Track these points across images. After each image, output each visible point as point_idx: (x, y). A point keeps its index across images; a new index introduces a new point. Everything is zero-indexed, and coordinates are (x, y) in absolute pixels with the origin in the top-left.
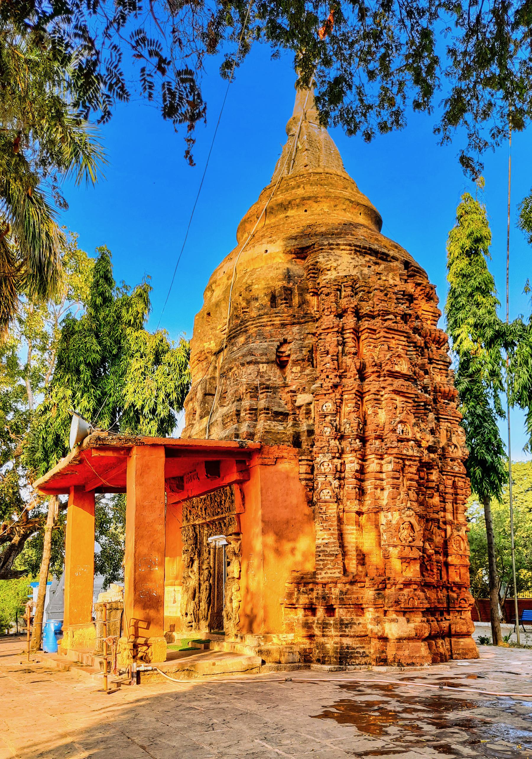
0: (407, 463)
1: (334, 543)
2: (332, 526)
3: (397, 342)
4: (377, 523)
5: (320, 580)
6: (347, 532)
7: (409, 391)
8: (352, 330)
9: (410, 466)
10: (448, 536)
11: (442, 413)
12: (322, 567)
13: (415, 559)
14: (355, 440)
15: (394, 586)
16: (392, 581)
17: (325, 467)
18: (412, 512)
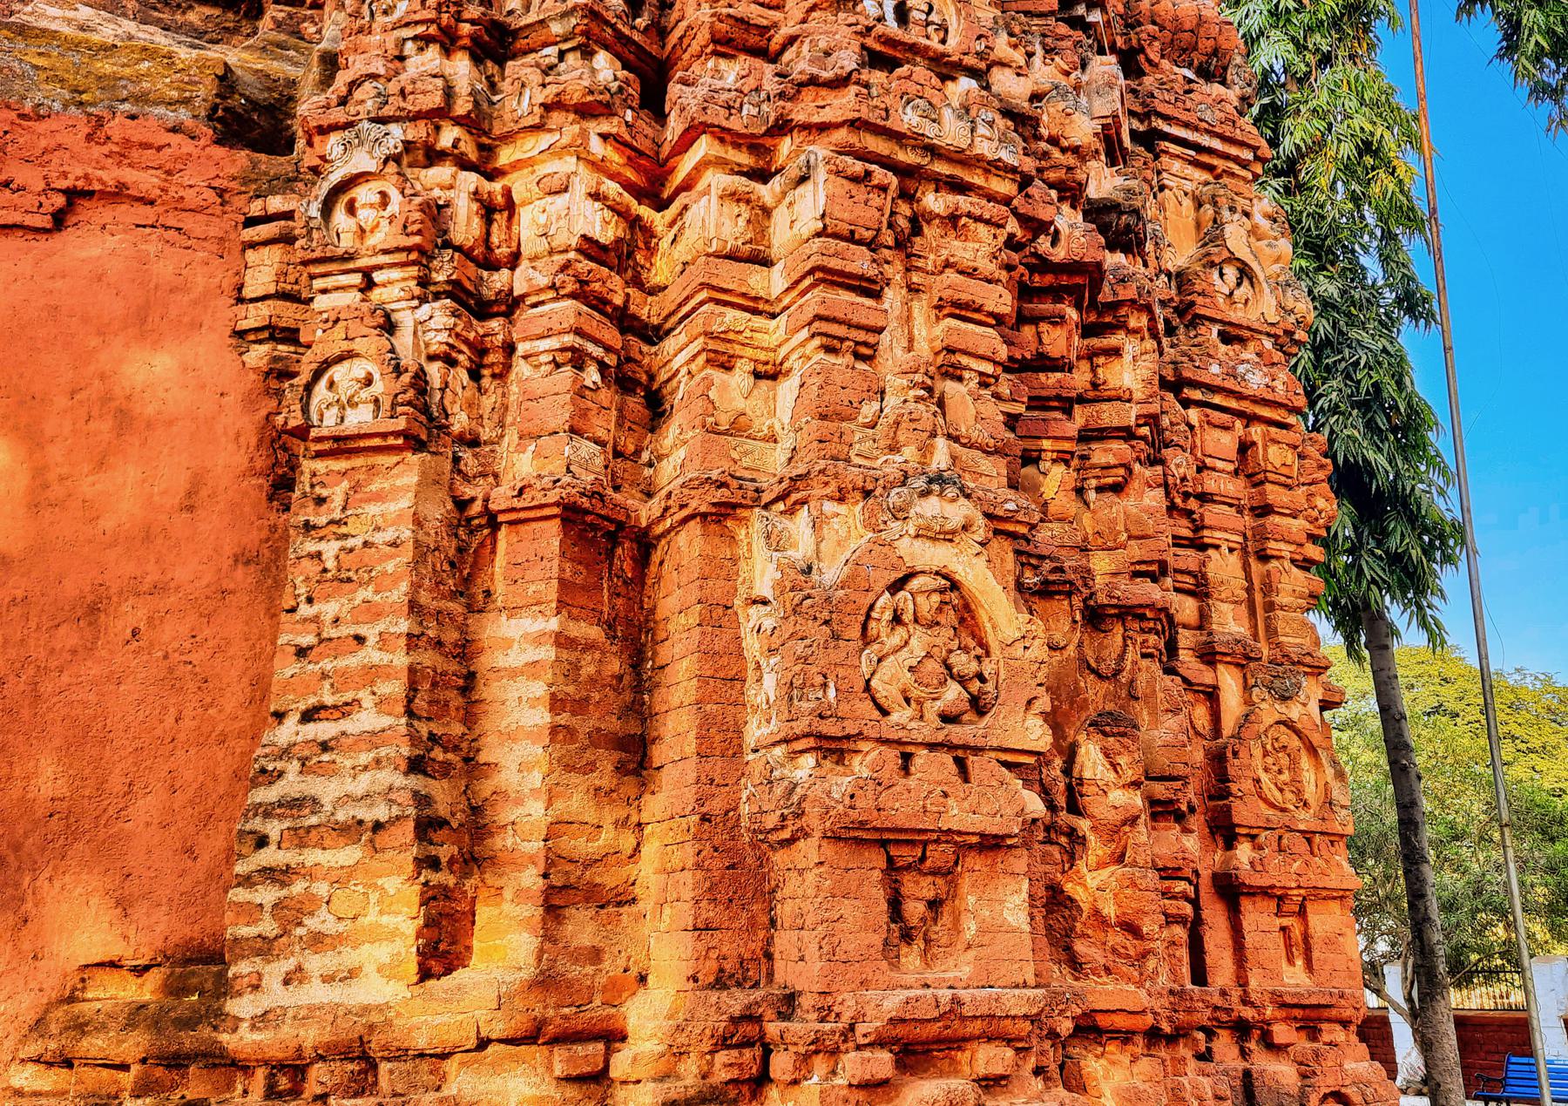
0: (934, 202)
1: (373, 738)
2: (372, 612)
4: (717, 589)
5: (242, 1040)
6: (501, 661)
9: (952, 220)
10: (1228, 724)
11: (1162, 108)
12: (268, 927)
13: (991, 844)
14: (588, 54)
15: (820, 1065)
16: (803, 1027)
17: (366, 215)
18: (957, 512)
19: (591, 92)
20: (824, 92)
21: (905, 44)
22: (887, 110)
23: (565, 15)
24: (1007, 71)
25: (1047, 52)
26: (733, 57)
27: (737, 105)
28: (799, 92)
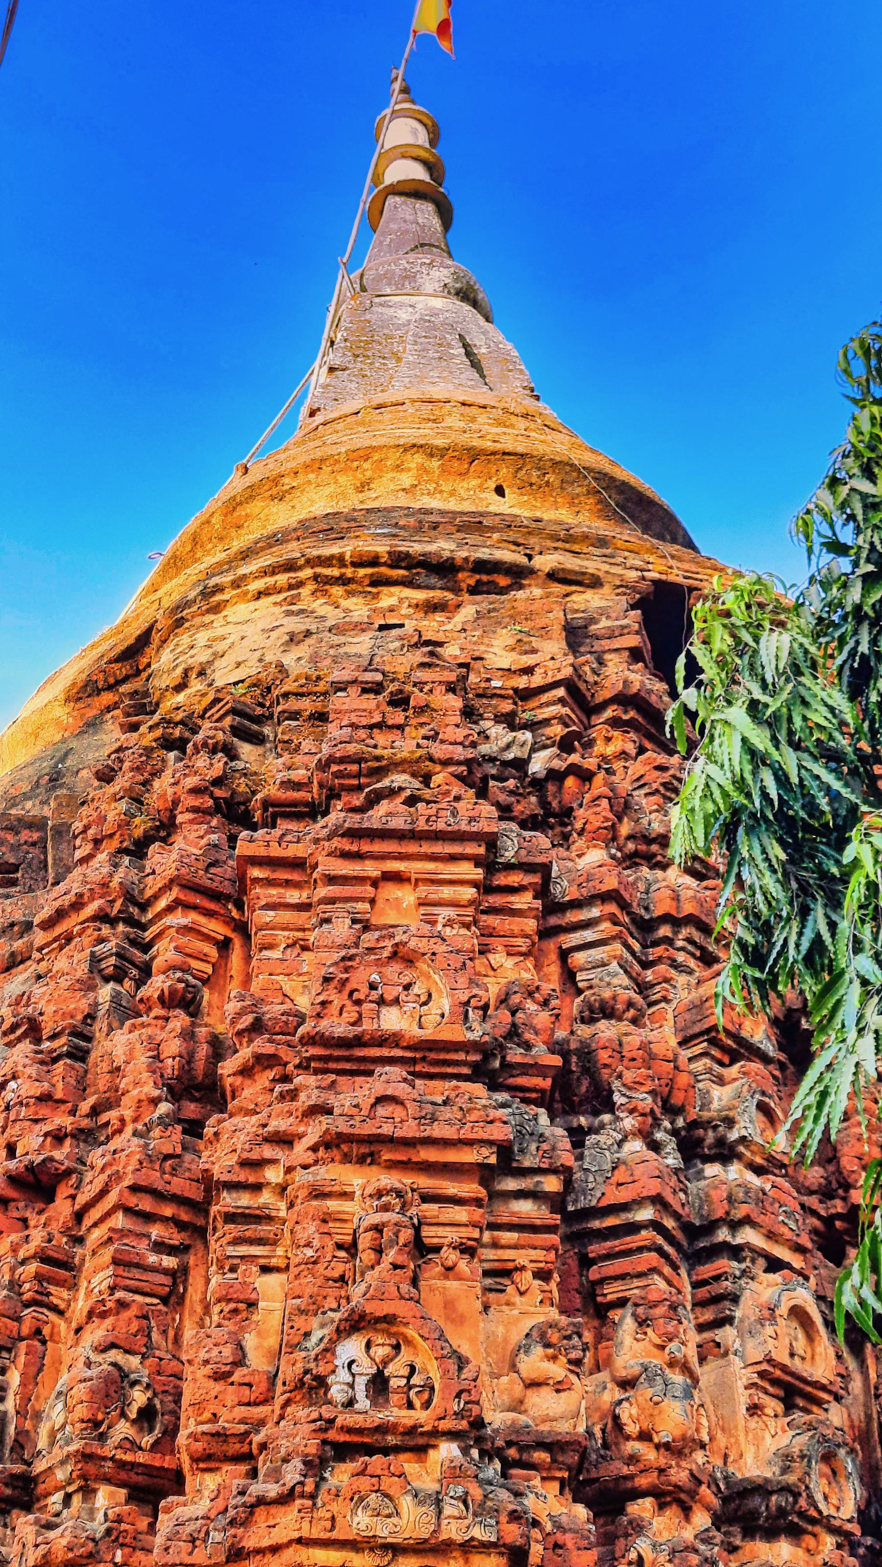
3: (423, 890)
7: (438, 1131)
8: (175, 893)
14: (88, 1492)
19: (71, 1550)
20: (273, 1510)
21: (369, 1429)
22: (333, 1519)
23: (63, 1463)
24: (545, 1391)
25: (640, 1324)
26: (218, 1469)
27: (202, 1535)
28: (252, 1513)
